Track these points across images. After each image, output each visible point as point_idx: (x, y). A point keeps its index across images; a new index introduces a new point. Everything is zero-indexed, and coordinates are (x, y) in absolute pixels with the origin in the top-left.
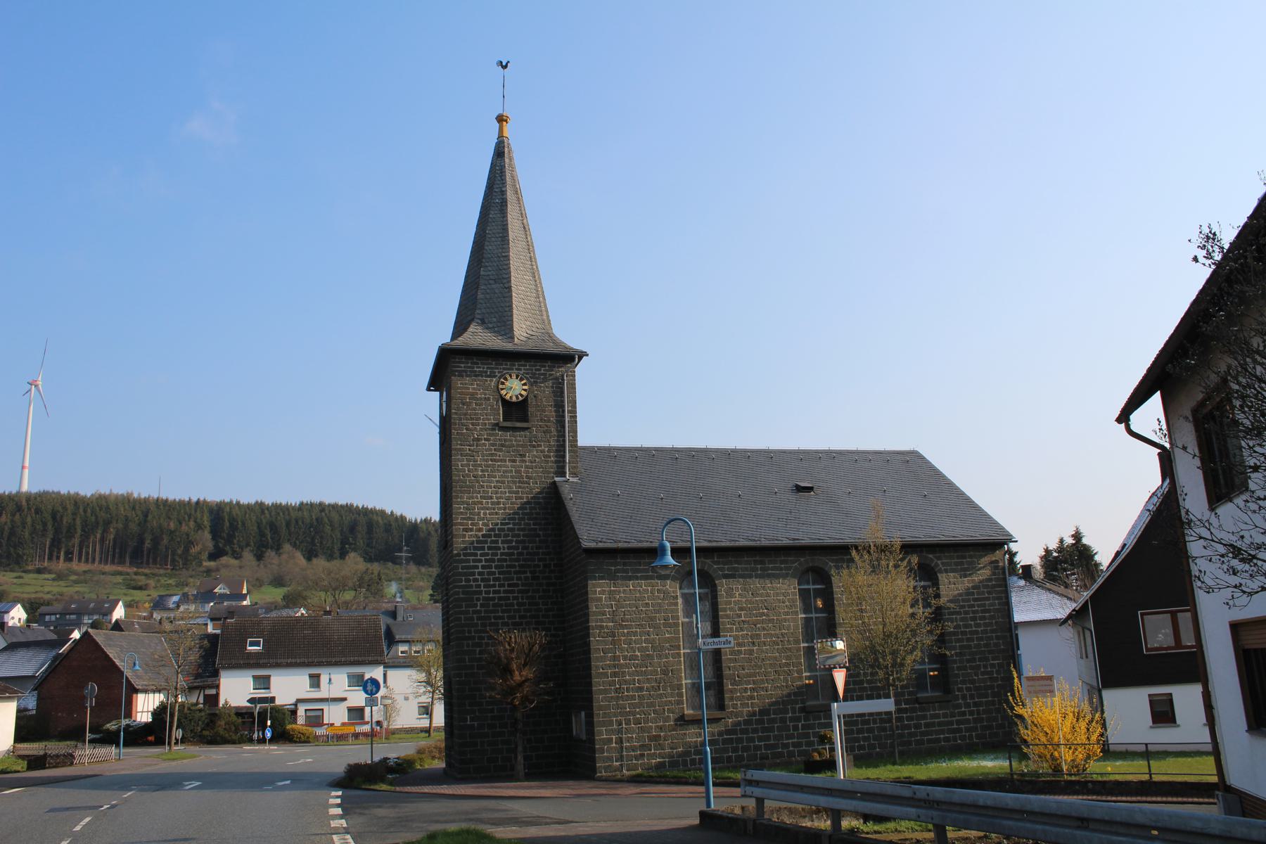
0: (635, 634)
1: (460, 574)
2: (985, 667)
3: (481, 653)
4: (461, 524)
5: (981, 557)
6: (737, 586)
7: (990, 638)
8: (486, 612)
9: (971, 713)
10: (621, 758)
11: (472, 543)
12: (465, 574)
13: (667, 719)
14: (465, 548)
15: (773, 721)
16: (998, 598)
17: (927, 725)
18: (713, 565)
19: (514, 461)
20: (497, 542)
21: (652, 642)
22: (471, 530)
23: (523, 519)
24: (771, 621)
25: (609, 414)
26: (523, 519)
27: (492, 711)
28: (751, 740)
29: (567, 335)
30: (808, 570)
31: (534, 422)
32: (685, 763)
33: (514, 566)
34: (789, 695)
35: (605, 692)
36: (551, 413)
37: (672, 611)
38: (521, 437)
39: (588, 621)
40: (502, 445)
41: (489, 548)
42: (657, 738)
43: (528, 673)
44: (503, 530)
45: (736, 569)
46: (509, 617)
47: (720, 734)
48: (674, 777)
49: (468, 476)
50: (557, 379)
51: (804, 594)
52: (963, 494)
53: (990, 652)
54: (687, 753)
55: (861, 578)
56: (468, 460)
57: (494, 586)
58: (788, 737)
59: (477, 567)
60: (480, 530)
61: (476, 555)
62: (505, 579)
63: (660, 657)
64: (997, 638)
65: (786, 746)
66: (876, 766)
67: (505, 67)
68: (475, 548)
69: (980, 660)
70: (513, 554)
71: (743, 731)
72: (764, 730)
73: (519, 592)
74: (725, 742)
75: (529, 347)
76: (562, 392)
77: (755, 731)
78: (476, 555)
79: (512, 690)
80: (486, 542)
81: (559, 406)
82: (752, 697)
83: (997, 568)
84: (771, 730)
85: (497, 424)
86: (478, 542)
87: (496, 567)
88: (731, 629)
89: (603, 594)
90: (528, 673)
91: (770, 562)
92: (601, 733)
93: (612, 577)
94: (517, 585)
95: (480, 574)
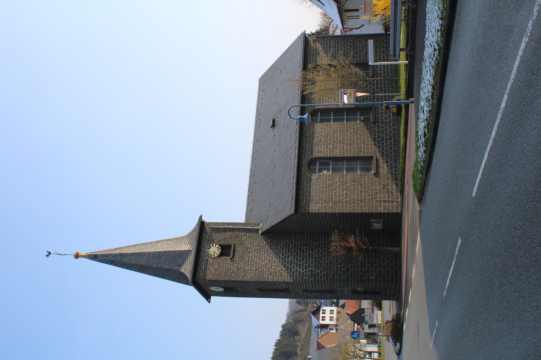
0: (336, 193)
1: (302, 279)
2: (360, 48)
3: (340, 271)
4: (278, 278)
5: (311, 46)
6: (316, 149)
7: (347, 45)
8: (321, 268)
9: (380, 55)
10: (393, 201)
11: (288, 273)
12: (303, 277)
13: (376, 181)
14: (290, 276)
15: (379, 136)
16: (330, 40)
17: (384, 73)
18: (307, 163)
19: (250, 252)
20: (288, 261)
21: (340, 186)
22: (281, 273)
23: (278, 249)
24: (333, 135)
25: (230, 207)
26: (278, 249)
27: (368, 267)
28: (387, 146)
29: (190, 226)
30: (309, 168)
31: (231, 242)
32: (396, 174)
33: (300, 254)
34: (367, 129)
35: (361, 207)
36: (228, 234)
37: (326, 177)
38: (239, 249)
39: (328, 213)
40: (242, 257)
41: (291, 265)
42: (384, 186)
43: (351, 239)
44: (282, 258)
45: (309, 149)
46: (325, 257)
47: (384, 159)
48: (402, 174)
49: (255, 273)
50: (211, 231)
51: (322, 121)
52: (281, 56)
53: (354, 45)
54: (392, 173)
55: (317, 88)
56: (248, 273)
57: (309, 264)
58: (386, 130)
59: (300, 271)
60: (282, 269)
61: (294, 272)
62: (306, 259)
63: (347, 183)
64: (347, 42)
65: (390, 132)
66: (400, 70)
67: (50, 253)
68: (290, 271)
69: (357, 49)
70: (294, 254)
71: (383, 149)
72: (382, 140)
73: (312, 252)
74: (387, 157)
75: (195, 243)
76: (218, 228)
77: (383, 144)
78: (294, 272)
79: (360, 249)
80: (288, 266)
81: (225, 230)
82: (368, 145)
83: (316, 40)
84: (383, 137)
85: (231, 259)
86: (287, 270)
87: (300, 262)
88: (336, 152)
89: (316, 206)
90: (351, 239)
91: (307, 134)
92: (380, 210)
93: (309, 201)
94: (309, 254)
95: (303, 270)
